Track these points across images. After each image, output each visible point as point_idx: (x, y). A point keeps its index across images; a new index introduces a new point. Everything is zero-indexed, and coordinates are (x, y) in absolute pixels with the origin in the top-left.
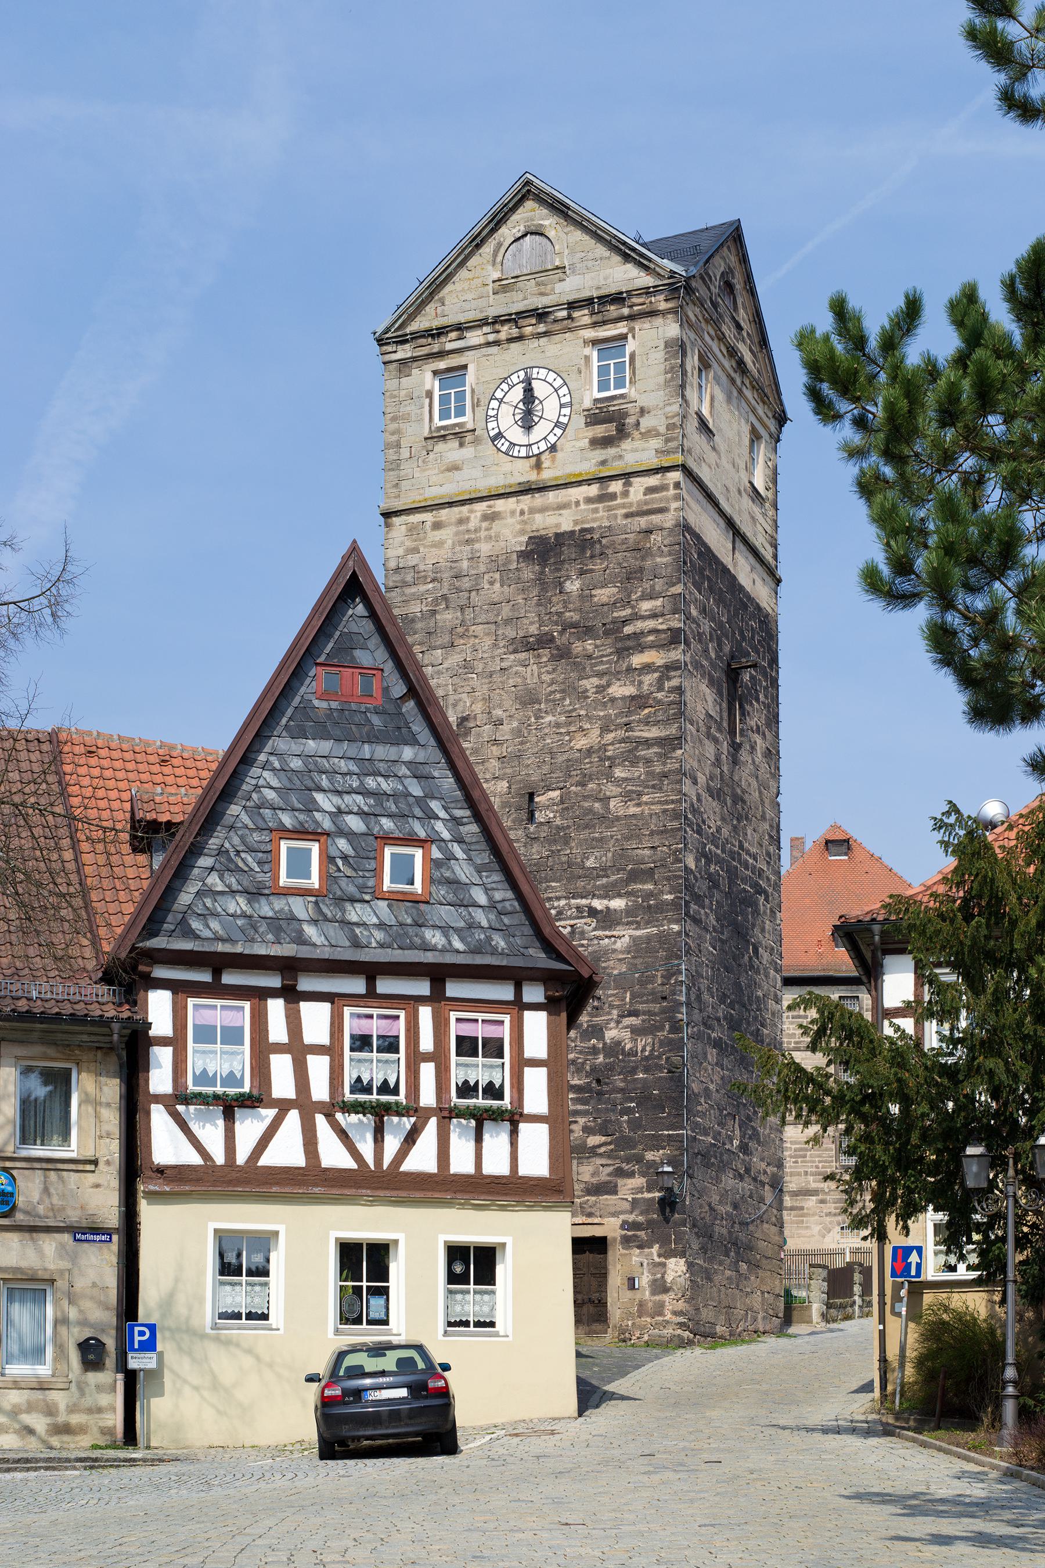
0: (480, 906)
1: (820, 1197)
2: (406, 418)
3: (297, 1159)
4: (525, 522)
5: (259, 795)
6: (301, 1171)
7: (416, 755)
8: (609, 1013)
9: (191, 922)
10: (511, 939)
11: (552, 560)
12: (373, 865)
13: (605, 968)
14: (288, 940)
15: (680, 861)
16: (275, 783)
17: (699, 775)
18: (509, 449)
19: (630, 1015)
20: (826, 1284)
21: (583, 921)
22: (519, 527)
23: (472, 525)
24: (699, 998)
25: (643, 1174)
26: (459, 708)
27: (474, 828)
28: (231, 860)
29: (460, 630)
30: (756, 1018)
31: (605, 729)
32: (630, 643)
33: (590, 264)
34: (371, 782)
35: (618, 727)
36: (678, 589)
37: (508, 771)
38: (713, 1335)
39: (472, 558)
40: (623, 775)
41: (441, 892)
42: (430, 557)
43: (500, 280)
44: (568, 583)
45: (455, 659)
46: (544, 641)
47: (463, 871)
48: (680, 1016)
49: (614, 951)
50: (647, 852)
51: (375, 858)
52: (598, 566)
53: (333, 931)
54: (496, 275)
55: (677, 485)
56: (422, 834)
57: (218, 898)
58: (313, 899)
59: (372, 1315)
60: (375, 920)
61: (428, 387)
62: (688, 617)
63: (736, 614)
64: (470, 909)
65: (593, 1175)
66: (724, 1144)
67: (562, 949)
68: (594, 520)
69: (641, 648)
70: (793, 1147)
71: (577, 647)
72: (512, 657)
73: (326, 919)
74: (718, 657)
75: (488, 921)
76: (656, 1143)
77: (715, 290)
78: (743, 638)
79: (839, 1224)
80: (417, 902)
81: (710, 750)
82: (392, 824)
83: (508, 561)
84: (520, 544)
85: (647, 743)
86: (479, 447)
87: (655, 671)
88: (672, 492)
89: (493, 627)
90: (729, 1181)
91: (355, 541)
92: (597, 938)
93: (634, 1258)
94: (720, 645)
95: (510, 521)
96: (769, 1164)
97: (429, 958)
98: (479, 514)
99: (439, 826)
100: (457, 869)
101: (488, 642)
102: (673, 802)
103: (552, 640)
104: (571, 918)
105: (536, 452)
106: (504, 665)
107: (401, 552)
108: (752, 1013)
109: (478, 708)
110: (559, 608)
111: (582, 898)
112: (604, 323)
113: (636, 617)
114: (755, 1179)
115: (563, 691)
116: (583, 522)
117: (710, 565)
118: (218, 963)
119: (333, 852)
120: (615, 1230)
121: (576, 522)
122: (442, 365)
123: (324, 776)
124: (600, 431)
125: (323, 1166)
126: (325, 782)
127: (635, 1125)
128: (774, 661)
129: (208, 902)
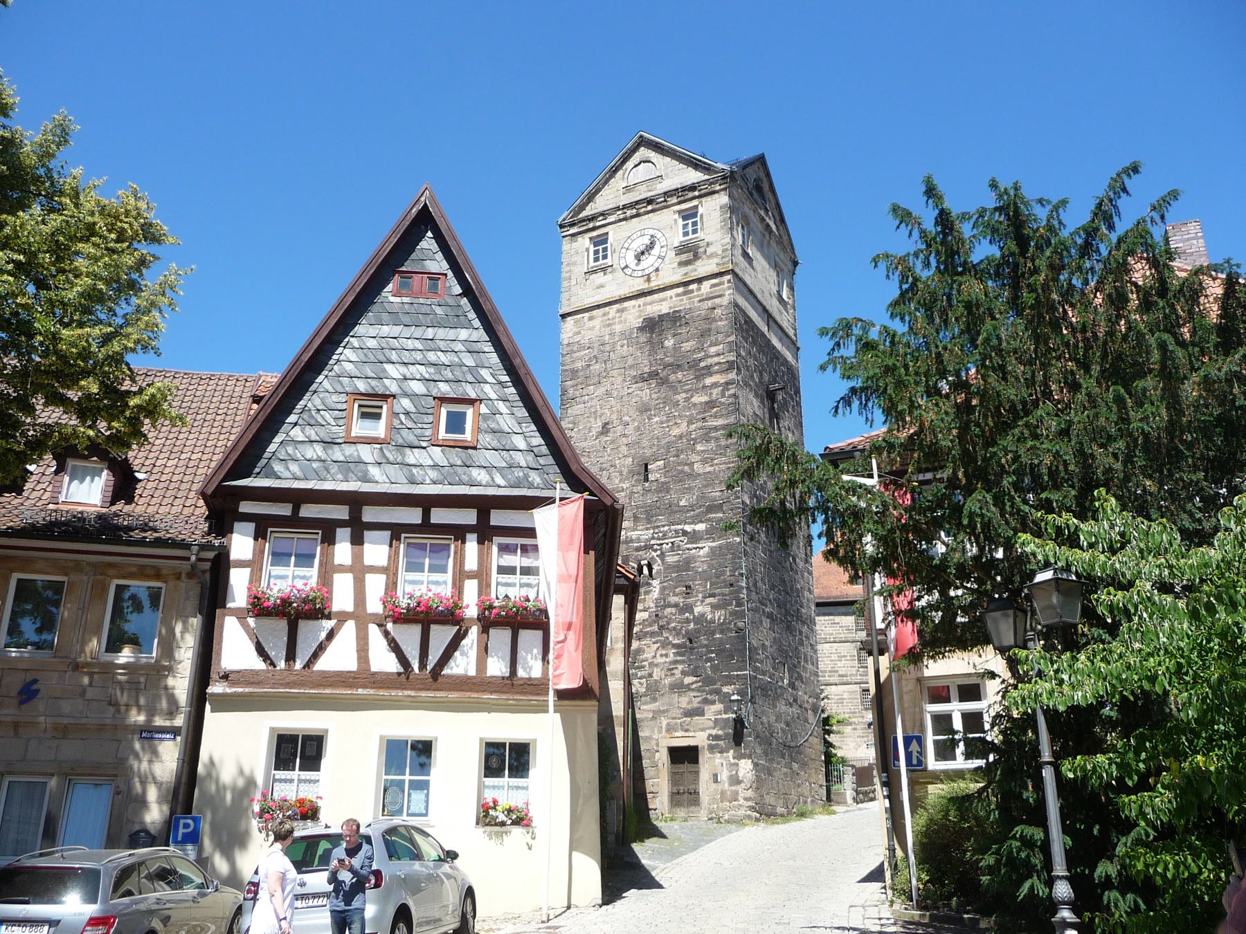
2: (575, 264)
3: (351, 664)
12: (431, 419)
16: (353, 357)
24: (755, 585)
25: (721, 702)
27: (513, 390)
28: (312, 417)
31: (690, 423)
34: (432, 357)
35: (698, 420)
36: (733, 338)
41: (486, 440)
45: (601, 391)
46: (653, 375)
52: (684, 330)
53: (391, 470)
55: (729, 281)
56: (473, 395)
59: (412, 810)
62: (739, 355)
63: (772, 360)
67: (588, 483)
71: (672, 378)
73: (389, 463)
76: (729, 681)
80: (466, 448)
83: (631, 333)
85: (716, 429)
88: (726, 285)
90: (782, 707)
91: (660, 887)
94: (761, 375)
99: (487, 388)
101: (620, 379)
107: (570, 334)
109: (614, 417)
110: (661, 356)
112: (685, 201)
118: (298, 497)
119: (397, 409)
122: (594, 234)
124: (684, 257)
126: (394, 356)
128: (797, 392)
129: (290, 450)
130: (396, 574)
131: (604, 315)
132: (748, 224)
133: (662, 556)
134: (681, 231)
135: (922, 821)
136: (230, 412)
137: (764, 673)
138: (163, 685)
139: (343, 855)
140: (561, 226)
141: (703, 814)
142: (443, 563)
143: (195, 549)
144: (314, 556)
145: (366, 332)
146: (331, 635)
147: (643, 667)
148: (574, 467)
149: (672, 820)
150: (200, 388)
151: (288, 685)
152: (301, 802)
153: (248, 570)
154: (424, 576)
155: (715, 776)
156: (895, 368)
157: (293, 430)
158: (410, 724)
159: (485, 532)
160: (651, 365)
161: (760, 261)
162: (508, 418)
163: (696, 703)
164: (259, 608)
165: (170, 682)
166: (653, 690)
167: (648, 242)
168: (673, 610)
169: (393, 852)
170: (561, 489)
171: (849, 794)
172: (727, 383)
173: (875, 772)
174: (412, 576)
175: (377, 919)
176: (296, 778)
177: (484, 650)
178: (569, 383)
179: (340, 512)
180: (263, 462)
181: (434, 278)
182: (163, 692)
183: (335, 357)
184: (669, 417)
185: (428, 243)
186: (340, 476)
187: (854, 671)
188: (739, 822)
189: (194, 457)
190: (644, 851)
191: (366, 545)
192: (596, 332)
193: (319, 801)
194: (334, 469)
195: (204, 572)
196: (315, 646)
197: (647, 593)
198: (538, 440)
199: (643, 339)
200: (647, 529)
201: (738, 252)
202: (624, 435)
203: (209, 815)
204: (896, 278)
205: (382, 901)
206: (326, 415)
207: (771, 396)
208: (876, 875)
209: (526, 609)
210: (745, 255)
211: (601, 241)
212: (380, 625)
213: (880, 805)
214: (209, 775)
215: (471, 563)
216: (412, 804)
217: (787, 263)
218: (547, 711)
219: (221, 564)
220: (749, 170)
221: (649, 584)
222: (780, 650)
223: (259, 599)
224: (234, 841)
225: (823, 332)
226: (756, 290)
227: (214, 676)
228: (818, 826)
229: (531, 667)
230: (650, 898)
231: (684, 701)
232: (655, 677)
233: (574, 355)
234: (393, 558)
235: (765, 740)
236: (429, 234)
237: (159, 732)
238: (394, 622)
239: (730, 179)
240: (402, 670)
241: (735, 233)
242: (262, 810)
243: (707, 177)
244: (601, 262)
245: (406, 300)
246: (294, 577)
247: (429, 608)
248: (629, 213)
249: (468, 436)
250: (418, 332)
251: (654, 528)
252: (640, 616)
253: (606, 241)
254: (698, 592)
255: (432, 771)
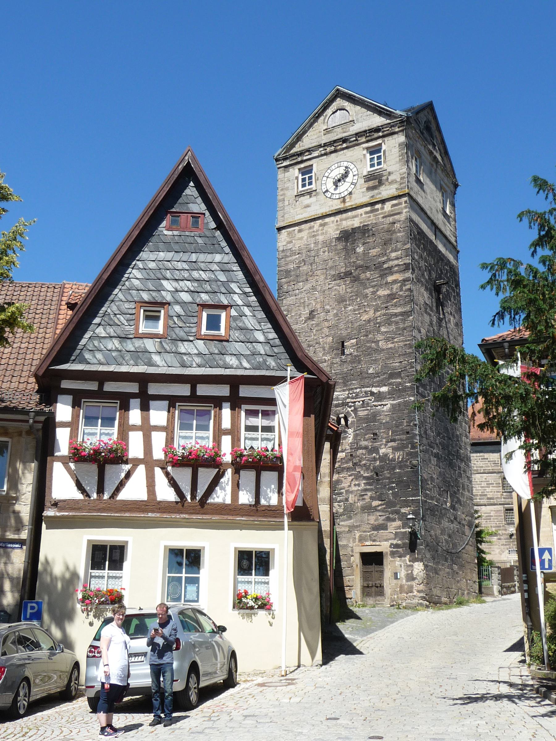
0: (261, 343)
1: (498, 537)
2: (287, 189)
3: (142, 495)
4: (338, 225)
5: (130, 283)
6: (144, 503)
7: (223, 258)
8: (381, 441)
9: (85, 354)
10: (279, 361)
11: (351, 240)
13: (379, 419)
14: (142, 363)
15: (413, 367)
16: (139, 276)
17: (422, 329)
18: (331, 196)
19: (392, 441)
20: (500, 576)
21: (368, 398)
22: (336, 227)
23: (315, 229)
24: (425, 432)
25: (400, 520)
26: (310, 307)
27: (254, 298)
29: (310, 273)
30: (456, 445)
31: (376, 310)
32: (386, 272)
33: (365, 118)
34: (195, 274)
36: (408, 246)
37: (332, 332)
38: (440, 603)
39: (315, 243)
40: (385, 330)
41: (236, 335)
42: (297, 245)
43: (326, 129)
44: (358, 249)
45: (308, 286)
46: (348, 274)
47: (250, 322)
48: (416, 441)
49: (383, 411)
50: (397, 364)
51: (197, 316)
52: (371, 240)
53: (169, 358)
54: (325, 128)
55: (406, 202)
56: (226, 302)
57: (102, 340)
58: (159, 340)
60: (196, 351)
61: (296, 175)
62: (413, 259)
63: (438, 262)
64: (254, 344)
65: (375, 521)
66: (442, 505)
67: (309, 365)
68: (369, 221)
69: (392, 274)
70: (485, 515)
71: (363, 276)
72: (333, 282)
74: (429, 278)
75: (265, 350)
76: (406, 504)
77: (422, 127)
78: (442, 273)
79: (507, 549)
80: (221, 341)
81: (427, 318)
82: (208, 297)
83: (331, 242)
84: (336, 234)
85: (396, 315)
86: (318, 197)
87: (398, 283)
88: (404, 205)
89: (325, 271)
90: (445, 523)
91: (361, 653)
92: (375, 406)
93: (397, 563)
94: (430, 273)
95: (332, 225)
96: (467, 516)
97: (228, 372)
98: (318, 224)
99: (236, 297)
100: (246, 321)
101: (322, 277)
102: (409, 340)
103: (351, 274)
104: (362, 397)
105: (343, 196)
106: (330, 286)
107: (285, 243)
108: (454, 443)
109: (318, 306)
111: (367, 387)
113: (389, 260)
114: (459, 523)
115: (356, 295)
116: (364, 222)
117: (424, 238)
118: (102, 377)
119: (171, 313)
120: (387, 548)
121: (361, 223)
122: (302, 166)
123: (168, 271)
124: (371, 183)
125: (158, 500)
126: (168, 274)
127: (395, 495)
128: (458, 285)
129: (96, 343)
130: (173, 432)
131: (310, 228)
132: (420, 157)
133: (355, 411)
134: (369, 163)
135: (552, 609)
136: (45, 312)
137: (432, 498)
138: (11, 509)
139: (157, 627)
140: (277, 160)
141: (387, 602)
142: (206, 423)
143: (32, 414)
144: (114, 419)
145: (148, 257)
146: (128, 475)
147: (341, 493)
148: (299, 355)
149: (364, 606)
150: (22, 293)
151: (99, 510)
152: (111, 591)
153: (68, 429)
154: (193, 433)
155: (396, 574)
156: (536, 300)
157: (98, 329)
158: (185, 538)
159: (236, 402)
160: (346, 266)
161: (429, 185)
162: (251, 319)
163: (381, 520)
164: (77, 455)
165: (17, 507)
166: (349, 511)
167: (343, 172)
168: (364, 451)
169: (186, 626)
170: (290, 371)
171: (496, 588)
172: (404, 280)
173: (515, 572)
174: (184, 433)
175: (180, 667)
176: (106, 575)
177: (237, 486)
178: (284, 280)
179: (133, 388)
180: (77, 352)
181: (196, 216)
182: (12, 515)
183: (126, 275)
184: (360, 306)
185: (191, 191)
186: (132, 362)
187: (499, 495)
188: (414, 608)
189: (23, 346)
190: (346, 628)
191: (152, 412)
192: (304, 241)
193: (122, 591)
194: (128, 357)
195: (38, 430)
196: (117, 483)
197: (345, 438)
198: (272, 335)
199: (340, 246)
200: (344, 391)
201: (413, 179)
202: (326, 320)
203: (46, 598)
204: (536, 228)
205: (181, 659)
206: (121, 318)
207: (437, 289)
208: (518, 646)
209: (266, 456)
210: (418, 181)
211: (307, 171)
212: (162, 468)
213: (517, 598)
214: (45, 570)
215: (226, 423)
216: (187, 593)
217: (449, 186)
218: (283, 529)
219: (49, 425)
220: (421, 115)
221: (346, 432)
222: (444, 481)
223: (78, 450)
224: (63, 616)
225: (484, 266)
226: (426, 207)
227: (47, 504)
228: (471, 611)
229: (271, 498)
230: (356, 661)
231: (372, 519)
232: (351, 501)
233: (288, 259)
234: (171, 420)
235: (433, 547)
236: (192, 184)
237: (11, 543)
238: (173, 466)
239: (406, 123)
240: (179, 500)
241: (410, 165)
242: (84, 597)
243: (388, 121)
244: (307, 187)
245: (176, 233)
246: (101, 434)
247: (198, 456)
248: (329, 149)
249: (222, 332)
250: (185, 257)
251: (349, 390)
252: (340, 455)
253: (310, 171)
254: (382, 438)
255: (202, 571)
